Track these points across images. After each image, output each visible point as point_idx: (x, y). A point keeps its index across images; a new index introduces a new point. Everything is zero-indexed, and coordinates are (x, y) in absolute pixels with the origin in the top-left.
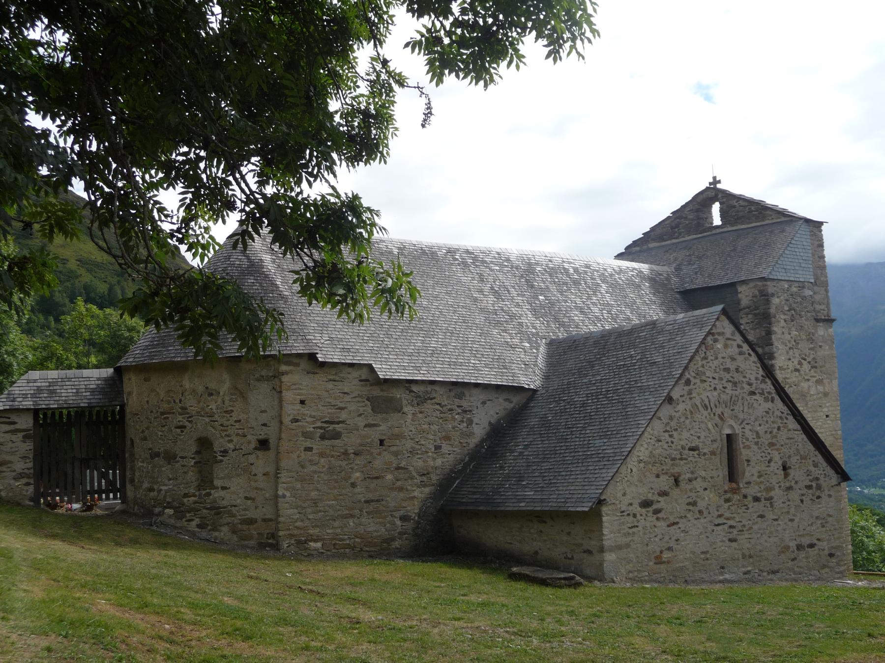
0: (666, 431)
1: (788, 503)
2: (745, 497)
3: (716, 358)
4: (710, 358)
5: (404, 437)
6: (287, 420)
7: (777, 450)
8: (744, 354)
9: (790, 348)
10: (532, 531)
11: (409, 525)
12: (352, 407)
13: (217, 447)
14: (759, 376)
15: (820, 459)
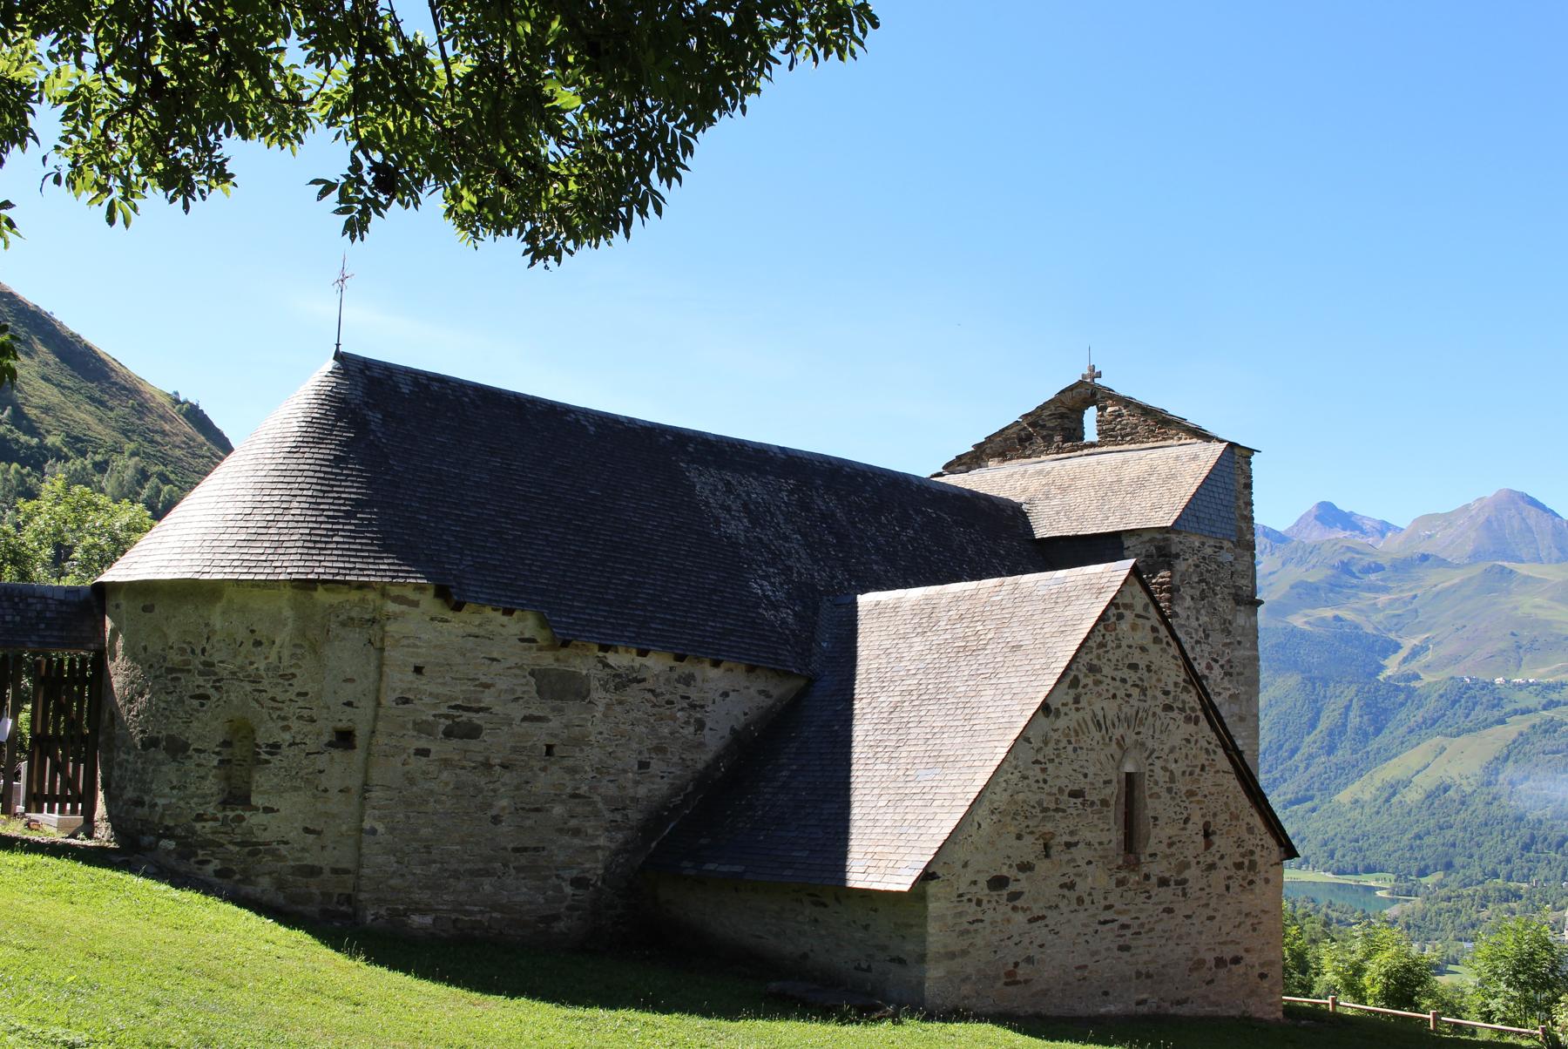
0: (1037, 762)
2: (1147, 877)
3: (1119, 646)
4: (1110, 645)
6: (388, 700)
7: (1198, 802)
9: (1197, 642)
10: (800, 918)
12: (502, 684)
13: (262, 738)
14: (1180, 680)
15: (1257, 821)
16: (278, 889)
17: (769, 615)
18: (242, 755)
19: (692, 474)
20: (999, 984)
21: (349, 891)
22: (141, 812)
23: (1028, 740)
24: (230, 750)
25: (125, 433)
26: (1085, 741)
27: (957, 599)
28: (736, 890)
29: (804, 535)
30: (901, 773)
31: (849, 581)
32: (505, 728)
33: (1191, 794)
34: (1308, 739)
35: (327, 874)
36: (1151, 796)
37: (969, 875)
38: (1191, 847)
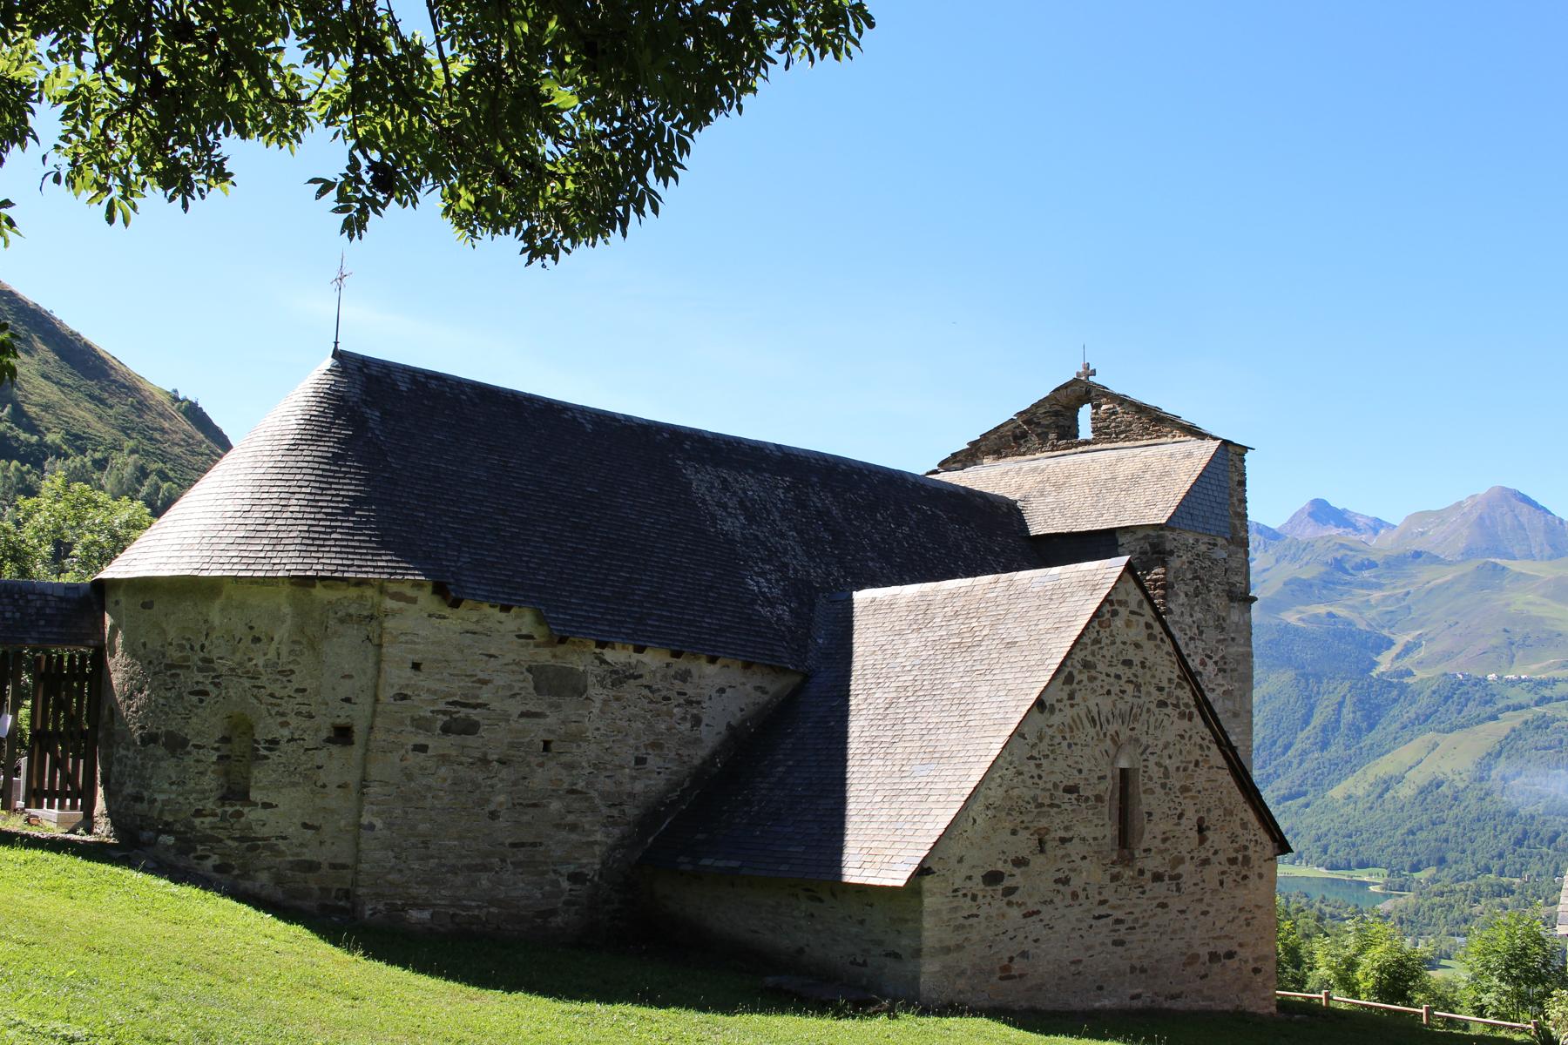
0: (1031, 758)
2: (1141, 872)
3: (1113, 643)
4: (1105, 641)
6: (386, 695)
7: (1193, 798)
9: (1191, 639)
10: (796, 913)
12: (500, 680)
14: (1174, 676)
15: (1251, 816)
18: (241, 752)
19: (689, 472)
20: (995, 979)
21: (347, 886)
23: (1023, 736)
25: (124, 430)
27: (953, 595)
31: (844, 577)
32: (503, 724)
34: (1301, 735)
37: (964, 871)
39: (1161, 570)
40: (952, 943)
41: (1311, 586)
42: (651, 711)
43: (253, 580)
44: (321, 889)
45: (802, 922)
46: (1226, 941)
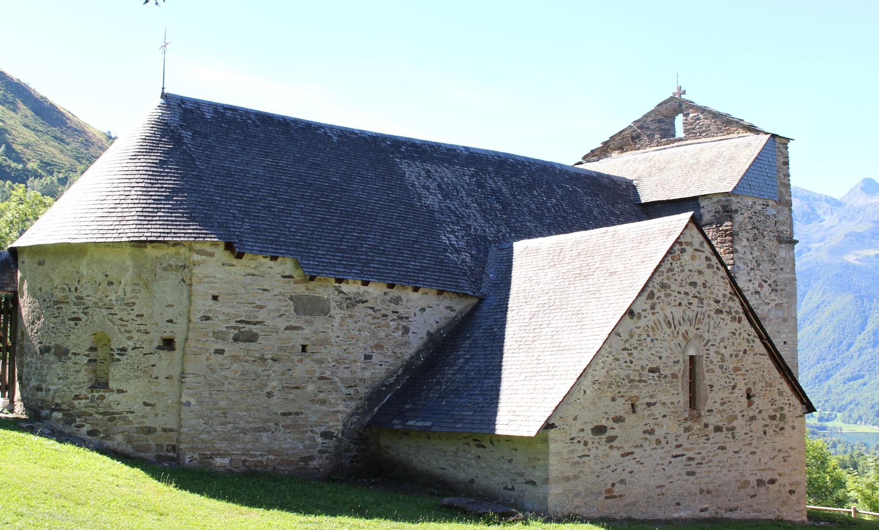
0: (625, 349)
1: (750, 434)
2: (706, 426)
3: (683, 271)
4: (676, 270)
5: (330, 344)
6: (196, 317)
7: (742, 375)
8: (713, 267)
9: (751, 269)
10: (469, 456)
11: (331, 443)
12: (271, 306)
14: (727, 293)
15: (786, 387)
16: (128, 442)
17: (454, 257)
18: (102, 357)
19: (404, 167)
20: (602, 498)
21: (174, 443)
22: (41, 395)
23: (619, 335)
24: (95, 353)
25: (77, 159)
26: (660, 335)
27: (577, 243)
28: (428, 438)
29: (479, 204)
30: (534, 358)
31: (510, 233)
32: (274, 335)
33: (736, 369)
34: (859, 337)
35: (159, 432)
36: (707, 371)
37: (578, 425)
38: (738, 404)
39: (729, 223)
40: (571, 474)
41: (863, 237)
42: (374, 326)
43: (107, 245)
44: (157, 445)
45: (473, 462)
46: (769, 472)
